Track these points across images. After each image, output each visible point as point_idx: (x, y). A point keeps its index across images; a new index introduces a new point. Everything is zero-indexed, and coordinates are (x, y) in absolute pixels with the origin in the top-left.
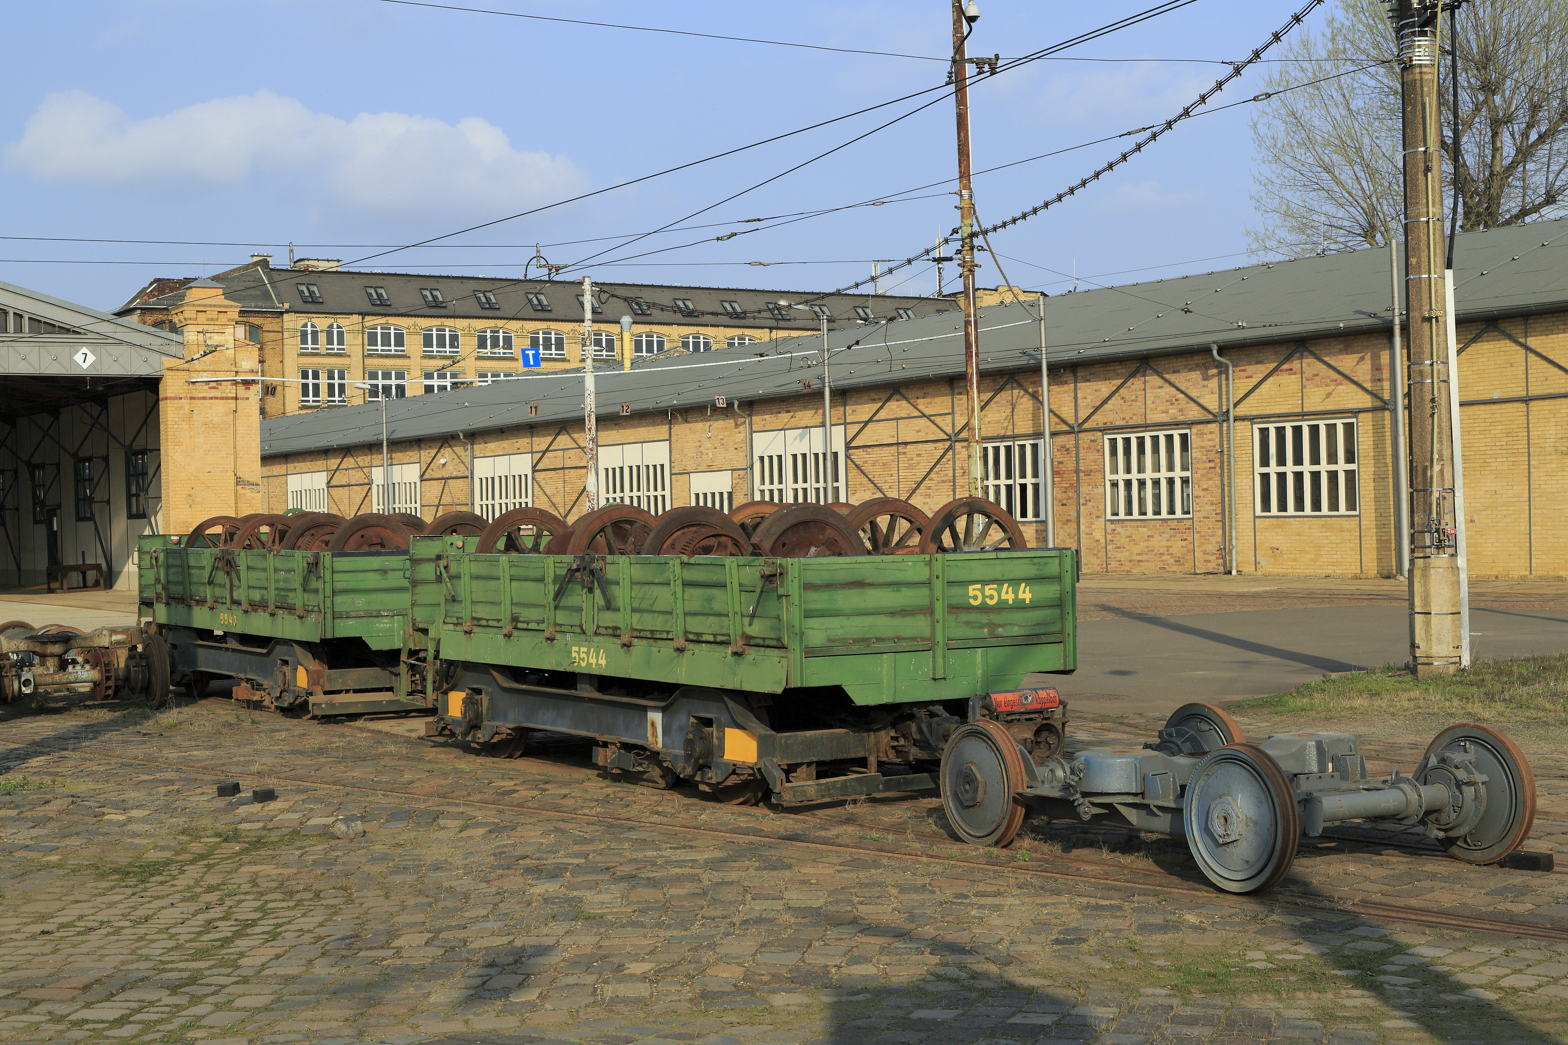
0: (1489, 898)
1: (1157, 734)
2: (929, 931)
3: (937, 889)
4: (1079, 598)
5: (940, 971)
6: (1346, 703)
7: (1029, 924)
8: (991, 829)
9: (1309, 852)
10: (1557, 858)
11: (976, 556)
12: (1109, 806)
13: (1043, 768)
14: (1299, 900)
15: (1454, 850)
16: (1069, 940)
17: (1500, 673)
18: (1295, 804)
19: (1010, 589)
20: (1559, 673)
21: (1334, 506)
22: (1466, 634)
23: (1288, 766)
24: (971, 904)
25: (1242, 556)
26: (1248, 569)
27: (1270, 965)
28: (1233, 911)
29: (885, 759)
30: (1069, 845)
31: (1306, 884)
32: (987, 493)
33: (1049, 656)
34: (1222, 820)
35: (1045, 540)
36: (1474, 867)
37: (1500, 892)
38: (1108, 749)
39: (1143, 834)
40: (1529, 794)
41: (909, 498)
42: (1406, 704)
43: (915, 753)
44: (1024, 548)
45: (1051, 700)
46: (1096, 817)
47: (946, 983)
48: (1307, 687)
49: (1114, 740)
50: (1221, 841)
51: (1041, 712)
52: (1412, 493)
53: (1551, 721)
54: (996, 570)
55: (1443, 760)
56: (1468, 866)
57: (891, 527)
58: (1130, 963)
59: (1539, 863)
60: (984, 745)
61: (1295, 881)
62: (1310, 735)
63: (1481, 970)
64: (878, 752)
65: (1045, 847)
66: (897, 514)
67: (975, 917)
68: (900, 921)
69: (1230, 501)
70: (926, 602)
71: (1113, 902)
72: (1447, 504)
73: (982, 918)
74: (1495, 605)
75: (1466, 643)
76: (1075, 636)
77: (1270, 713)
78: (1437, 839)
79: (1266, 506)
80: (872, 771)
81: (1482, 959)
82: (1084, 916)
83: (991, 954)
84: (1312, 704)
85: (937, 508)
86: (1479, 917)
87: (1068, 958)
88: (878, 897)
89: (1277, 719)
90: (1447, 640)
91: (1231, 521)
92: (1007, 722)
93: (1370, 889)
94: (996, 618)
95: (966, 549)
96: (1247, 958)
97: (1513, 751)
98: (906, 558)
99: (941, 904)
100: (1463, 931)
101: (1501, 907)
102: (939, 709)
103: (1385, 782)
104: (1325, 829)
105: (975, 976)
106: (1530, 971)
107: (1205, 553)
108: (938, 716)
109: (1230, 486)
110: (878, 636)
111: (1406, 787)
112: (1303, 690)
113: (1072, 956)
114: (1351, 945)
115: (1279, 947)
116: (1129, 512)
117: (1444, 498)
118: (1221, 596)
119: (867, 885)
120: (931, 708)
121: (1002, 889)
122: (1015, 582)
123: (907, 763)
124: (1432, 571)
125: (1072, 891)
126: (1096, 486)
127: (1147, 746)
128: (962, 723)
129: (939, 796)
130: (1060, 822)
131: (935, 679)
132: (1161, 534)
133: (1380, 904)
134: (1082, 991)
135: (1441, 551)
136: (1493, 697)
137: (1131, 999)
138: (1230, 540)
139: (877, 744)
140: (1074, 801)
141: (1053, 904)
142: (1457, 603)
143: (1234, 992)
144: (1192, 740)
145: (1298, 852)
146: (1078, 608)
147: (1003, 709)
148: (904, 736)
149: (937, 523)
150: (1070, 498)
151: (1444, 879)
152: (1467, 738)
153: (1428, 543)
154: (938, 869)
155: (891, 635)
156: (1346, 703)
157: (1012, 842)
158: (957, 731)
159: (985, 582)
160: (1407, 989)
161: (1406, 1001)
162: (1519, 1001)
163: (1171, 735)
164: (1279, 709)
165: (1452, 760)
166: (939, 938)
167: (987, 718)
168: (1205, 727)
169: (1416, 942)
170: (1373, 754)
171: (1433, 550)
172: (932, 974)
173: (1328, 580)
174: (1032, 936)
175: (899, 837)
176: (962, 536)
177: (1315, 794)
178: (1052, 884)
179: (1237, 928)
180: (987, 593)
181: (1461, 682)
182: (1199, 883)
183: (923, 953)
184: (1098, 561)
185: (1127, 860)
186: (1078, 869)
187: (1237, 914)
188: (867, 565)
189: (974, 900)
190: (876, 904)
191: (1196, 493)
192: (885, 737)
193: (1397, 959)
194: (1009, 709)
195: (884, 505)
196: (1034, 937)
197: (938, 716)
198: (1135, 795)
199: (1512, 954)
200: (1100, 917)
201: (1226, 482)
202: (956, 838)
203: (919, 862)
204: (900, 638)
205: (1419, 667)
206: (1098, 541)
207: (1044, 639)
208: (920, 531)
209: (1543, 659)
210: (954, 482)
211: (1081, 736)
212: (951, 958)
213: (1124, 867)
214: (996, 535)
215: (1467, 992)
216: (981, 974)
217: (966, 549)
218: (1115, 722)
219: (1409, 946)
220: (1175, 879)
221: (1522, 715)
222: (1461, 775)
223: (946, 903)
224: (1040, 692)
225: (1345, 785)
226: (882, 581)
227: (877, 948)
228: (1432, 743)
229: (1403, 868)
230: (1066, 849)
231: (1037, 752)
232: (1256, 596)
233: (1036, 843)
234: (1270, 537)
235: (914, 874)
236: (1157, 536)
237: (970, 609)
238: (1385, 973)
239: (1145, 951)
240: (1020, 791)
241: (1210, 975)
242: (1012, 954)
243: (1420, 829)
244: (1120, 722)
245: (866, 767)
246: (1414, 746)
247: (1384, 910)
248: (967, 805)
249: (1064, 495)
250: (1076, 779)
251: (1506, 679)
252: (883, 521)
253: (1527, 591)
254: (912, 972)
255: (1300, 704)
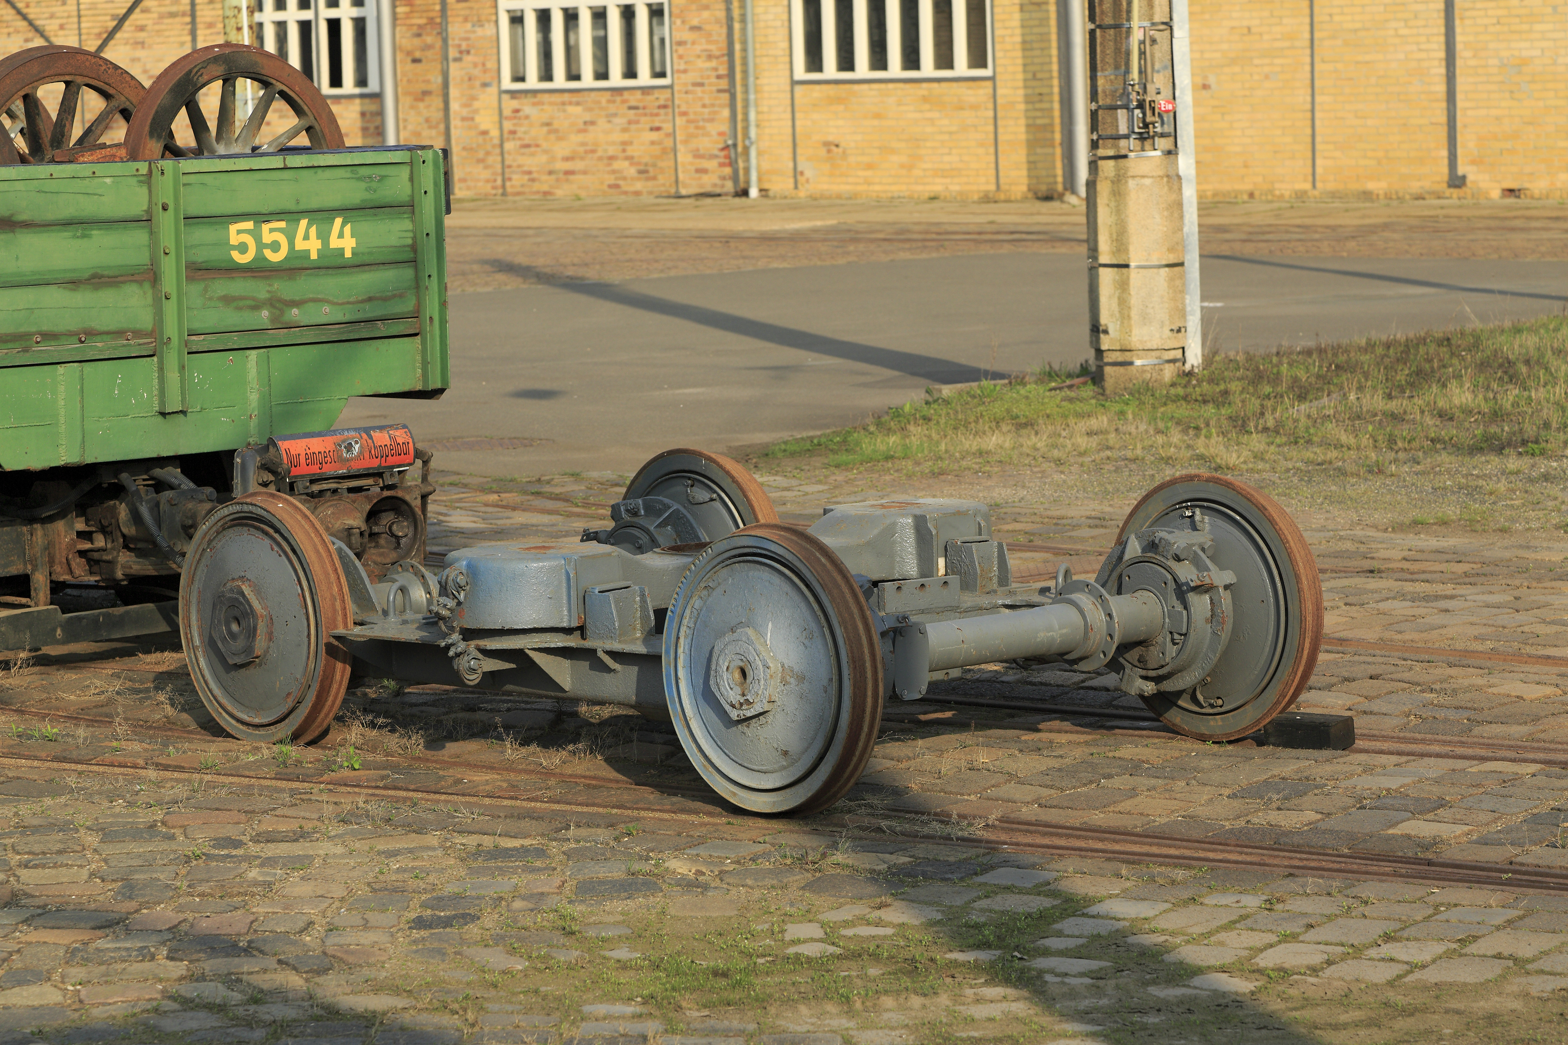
0: (1236, 803)
1: (608, 512)
2: (164, 913)
3: (177, 832)
4: (450, 248)
5: (189, 990)
6: (971, 443)
7: (363, 891)
8: (284, 710)
9: (903, 731)
10: (1360, 724)
11: (243, 164)
12: (517, 655)
13: (384, 586)
14: (884, 824)
15: (1174, 716)
16: (443, 918)
17: (1258, 378)
18: (876, 638)
19: (313, 231)
20: (1366, 375)
21: (945, 59)
22: (1194, 305)
23: (862, 566)
24: (248, 859)
25: (768, 163)
26: (781, 185)
27: (831, 949)
28: (759, 848)
29: (65, 577)
30: (440, 734)
31: (897, 792)
32: (260, 38)
33: (393, 363)
34: (737, 675)
35: (380, 131)
36: (1209, 746)
37: (1256, 792)
38: (512, 546)
39: (583, 709)
40: (1309, 606)
41: (101, 48)
42: (1083, 442)
43: (127, 564)
44: (337, 145)
45: (399, 450)
46: (491, 677)
47: (202, 1014)
48: (897, 413)
49: (525, 526)
50: (734, 714)
51: (380, 475)
52: (1092, 33)
53: (1350, 468)
54: (283, 192)
55: (1152, 546)
56: (1198, 746)
57: (68, 107)
58: (562, 957)
59: (1327, 735)
60: (267, 542)
61: (876, 788)
62: (903, 505)
63: (1220, 937)
64: (51, 562)
65: (393, 741)
66: (79, 80)
67: (256, 883)
68: (103, 895)
69: (744, 50)
70: (143, 258)
71: (527, 842)
72: (1159, 53)
73: (270, 884)
74: (1248, 250)
75: (1194, 323)
76: (443, 322)
77: (827, 466)
78: (1142, 696)
79: (814, 60)
80: (40, 602)
81: (1225, 918)
82: (472, 871)
83: (290, 953)
84: (906, 447)
85: (159, 68)
86: (1220, 841)
87: (442, 953)
88: (60, 852)
89: (839, 477)
90: (1158, 317)
91: (746, 91)
92: (312, 495)
93: (1017, 797)
94: (285, 288)
95: (221, 149)
96: (788, 937)
97: (1282, 524)
98: (99, 169)
99: (188, 860)
100: (1189, 867)
101: (1259, 819)
102: (174, 474)
103: (1044, 591)
104: (933, 686)
105: (258, 997)
106: (1311, 935)
107: (697, 155)
108: (171, 487)
109: (743, 20)
110: (45, 328)
111: (1084, 599)
112: (888, 420)
113: (450, 950)
114: (984, 903)
115: (847, 913)
116: (547, 74)
117: (1154, 41)
118: (728, 239)
119: (36, 830)
120: (158, 472)
121: (308, 826)
122: (322, 215)
123: (112, 584)
124: (1131, 183)
125: (448, 825)
126: (480, 23)
127: (589, 536)
128: (221, 501)
129: (177, 647)
130: (420, 689)
131: (163, 414)
132: (610, 117)
133: (1037, 824)
134: (470, 1016)
135: (1148, 144)
136: (1244, 425)
137: (565, 1026)
138: (746, 129)
139: (49, 547)
140: (448, 647)
141: (411, 851)
142: (1178, 245)
143: (763, 1002)
144: (676, 520)
145: (882, 732)
146: (449, 267)
147: (304, 469)
148: (104, 530)
149: (163, 97)
150: (428, 47)
151: (1156, 772)
152: (1196, 502)
153: (1123, 129)
154: (180, 791)
155: (73, 327)
156: (971, 443)
157: (325, 733)
158: (212, 516)
159: (261, 217)
160: (1087, 981)
161: (1085, 1004)
162: (1293, 992)
163: (634, 513)
164: (844, 457)
165: (1168, 543)
166: (184, 927)
167: (272, 489)
168: (701, 494)
169: (1105, 893)
170: (1022, 539)
171: (1133, 143)
172: (172, 998)
173: (936, 204)
174: (369, 915)
175: (98, 731)
176: (212, 126)
177: (914, 619)
178: (406, 813)
179: (769, 882)
180: (267, 238)
181: (1185, 398)
182: (694, 798)
183: (153, 958)
184: (486, 174)
185: (553, 759)
186: (459, 781)
187: (766, 855)
188: (19, 186)
189: (254, 849)
190: (55, 866)
191: (678, 36)
192: (64, 533)
193: (1068, 925)
194: (315, 469)
195: (51, 60)
196: (374, 917)
197: (171, 487)
198: (568, 631)
199: (1279, 907)
200: (502, 871)
201: (736, 13)
202: (216, 730)
203: (141, 780)
204: (91, 333)
205: (1108, 370)
206: (485, 133)
207: (383, 329)
208: (126, 114)
209: (1337, 349)
210: (193, 15)
211: (460, 520)
212: (210, 965)
213: (548, 773)
214: (281, 121)
215: (1196, 981)
216: (271, 993)
217: (221, 149)
218: (525, 493)
219: (1090, 901)
220: (648, 794)
221: (1298, 456)
222: (1186, 573)
223: (197, 857)
224: (376, 435)
225: (968, 600)
226: (50, 216)
227: (61, 953)
228: (1132, 514)
229: (1078, 753)
230: (434, 743)
231: (373, 554)
232: (795, 238)
233: (375, 732)
234: (825, 122)
235: (131, 804)
236: (602, 123)
237: (233, 270)
238: (1046, 952)
239: (591, 933)
240: (341, 631)
241: (716, 973)
242: (330, 951)
243: (1110, 680)
244: (536, 490)
245: (27, 595)
246: (1099, 521)
247: (1045, 834)
248: (235, 663)
249: (417, 41)
250: (451, 604)
251: (1268, 389)
252: (50, 95)
253: (1308, 221)
254: (132, 995)
255: (882, 448)
